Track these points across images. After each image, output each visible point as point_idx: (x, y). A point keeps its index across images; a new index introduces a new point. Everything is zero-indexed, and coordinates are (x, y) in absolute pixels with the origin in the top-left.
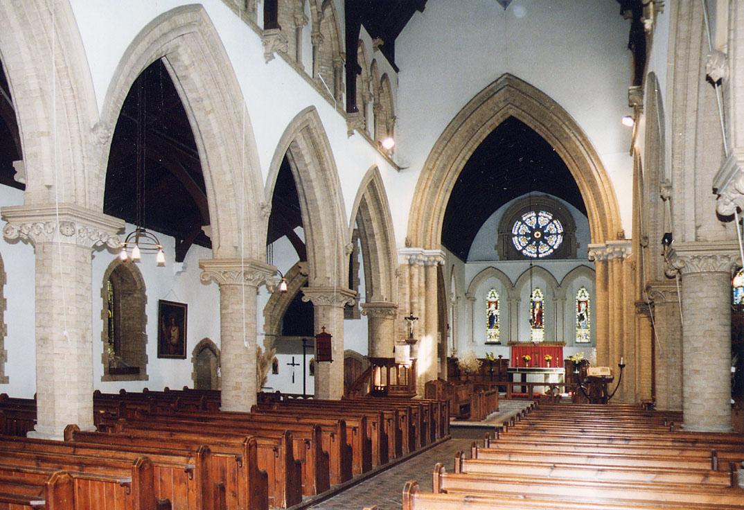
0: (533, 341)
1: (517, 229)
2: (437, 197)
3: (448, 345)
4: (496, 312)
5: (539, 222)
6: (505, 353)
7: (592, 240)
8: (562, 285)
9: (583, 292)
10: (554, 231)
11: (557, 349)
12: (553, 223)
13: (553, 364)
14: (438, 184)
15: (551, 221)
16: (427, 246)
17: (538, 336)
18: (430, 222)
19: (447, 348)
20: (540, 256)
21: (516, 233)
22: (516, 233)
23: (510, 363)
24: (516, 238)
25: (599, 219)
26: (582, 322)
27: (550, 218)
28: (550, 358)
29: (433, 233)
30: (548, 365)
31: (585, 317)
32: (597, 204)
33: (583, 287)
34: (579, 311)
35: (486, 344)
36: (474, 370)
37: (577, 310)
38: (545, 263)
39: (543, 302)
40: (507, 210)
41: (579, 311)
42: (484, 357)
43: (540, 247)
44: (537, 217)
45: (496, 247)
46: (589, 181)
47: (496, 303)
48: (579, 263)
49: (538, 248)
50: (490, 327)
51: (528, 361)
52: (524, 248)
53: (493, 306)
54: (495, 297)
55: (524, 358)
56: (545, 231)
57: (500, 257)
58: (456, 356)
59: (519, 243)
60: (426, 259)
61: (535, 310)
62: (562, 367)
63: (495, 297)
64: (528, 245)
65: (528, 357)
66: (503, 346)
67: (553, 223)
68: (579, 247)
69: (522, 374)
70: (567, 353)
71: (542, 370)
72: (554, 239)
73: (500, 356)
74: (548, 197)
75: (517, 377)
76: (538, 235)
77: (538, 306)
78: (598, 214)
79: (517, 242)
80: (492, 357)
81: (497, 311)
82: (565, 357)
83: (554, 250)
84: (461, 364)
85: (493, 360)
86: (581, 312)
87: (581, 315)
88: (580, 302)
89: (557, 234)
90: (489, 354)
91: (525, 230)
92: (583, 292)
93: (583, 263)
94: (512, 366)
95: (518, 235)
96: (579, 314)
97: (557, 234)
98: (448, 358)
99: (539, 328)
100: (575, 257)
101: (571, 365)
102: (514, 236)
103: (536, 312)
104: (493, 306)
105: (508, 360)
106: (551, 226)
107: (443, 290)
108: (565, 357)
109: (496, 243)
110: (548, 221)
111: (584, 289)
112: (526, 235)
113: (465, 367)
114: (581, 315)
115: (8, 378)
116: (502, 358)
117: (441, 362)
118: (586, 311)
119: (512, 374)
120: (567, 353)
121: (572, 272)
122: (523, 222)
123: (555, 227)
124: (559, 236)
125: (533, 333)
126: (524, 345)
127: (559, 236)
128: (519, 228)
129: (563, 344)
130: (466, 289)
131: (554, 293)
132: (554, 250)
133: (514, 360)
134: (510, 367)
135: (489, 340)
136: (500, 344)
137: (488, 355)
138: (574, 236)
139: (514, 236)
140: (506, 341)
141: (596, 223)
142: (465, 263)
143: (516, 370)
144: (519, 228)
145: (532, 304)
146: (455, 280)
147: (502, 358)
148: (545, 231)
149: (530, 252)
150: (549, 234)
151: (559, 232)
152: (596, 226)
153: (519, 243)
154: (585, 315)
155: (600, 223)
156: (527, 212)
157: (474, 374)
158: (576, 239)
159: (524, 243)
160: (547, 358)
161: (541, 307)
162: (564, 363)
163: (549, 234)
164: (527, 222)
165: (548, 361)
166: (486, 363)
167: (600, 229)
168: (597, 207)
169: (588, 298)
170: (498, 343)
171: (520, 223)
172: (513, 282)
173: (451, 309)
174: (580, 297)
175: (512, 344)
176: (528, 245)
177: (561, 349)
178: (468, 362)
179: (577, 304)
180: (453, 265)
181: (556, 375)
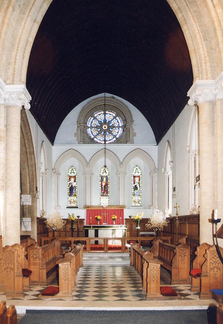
0: (102, 205)
1: (90, 123)
2: (23, 24)
3: (38, 206)
4: (74, 184)
5: (106, 118)
6: (82, 214)
7: (205, 77)
8: (123, 163)
9: (137, 169)
10: (116, 125)
11: (120, 211)
12: (116, 119)
13: (118, 223)
14: (45, 255)
15: (115, 117)
16: (8, 82)
17: (105, 202)
18: (14, 54)
19: (36, 209)
20: (107, 142)
21: (89, 126)
22: (89, 126)
23: (85, 221)
24: (89, 129)
25: (206, 54)
26: (136, 191)
27: (114, 115)
28: (116, 217)
29: (16, 67)
30: (99, 223)
31: (138, 187)
32: (204, 37)
33: (137, 166)
34: (134, 183)
35: (67, 208)
36: (59, 228)
37: (133, 182)
38: (111, 146)
39: (109, 176)
40: (84, 107)
41: (134, 183)
42: (66, 217)
43: (106, 136)
44: (105, 114)
45: (76, 135)
46: (195, 12)
47: (75, 177)
48: (136, 147)
49: (105, 137)
50: (70, 195)
51: (99, 220)
52: (95, 137)
53: (72, 179)
54: (74, 173)
55: (97, 218)
56: (110, 125)
57: (78, 142)
58: (44, 217)
59: (92, 133)
60: (7, 96)
61: (103, 182)
62: (123, 224)
63: (74, 173)
64: (98, 134)
65: (99, 217)
66: (80, 209)
67: (116, 119)
68: (135, 136)
69: (95, 230)
70: (127, 214)
71: (110, 227)
72: (117, 130)
73: (78, 217)
74: (114, 98)
75: (91, 233)
76: (105, 127)
77: (105, 179)
78: (205, 48)
79: (90, 132)
80: (73, 217)
81: (75, 183)
82: (126, 216)
83: (117, 139)
84: (48, 223)
85: (74, 219)
86: (136, 184)
87: (136, 186)
88: (134, 177)
89: (119, 127)
90: (71, 215)
91: (95, 123)
92: (137, 169)
93: (139, 147)
94: (87, 224)
95: (91, 127)
96: (134, 185)
97: (119, 127)
98: (38, 218)
99: (106, 196)
100: (133, 143)
101: (131, 222)
102: (89, 127)
103: (104, 184)
104: (72, 179)
105: (84, 220)
106: (115, 121)
107: (33, 157)
108: (126, 216)
109: (76, 132)
110: (113, 117)
111: (138, 167)
112: (97, 127)
113: (52, 225)
114: (136, 186)
115: (210, 222)
116: (80, 218)
117: (32, 221)
118: (139, 183)
119: (88, 230)
120: (127, 214)
121: (126, 158)
122: (95, 118)
123: (118, 122)
124: (120, 129)
125: (101, 199)
126: (97, 208)
127: (120, 129)
128: (92, 122)
129: (124, 207)
130: (53, 165)
131: (117, 169)
132: (117, 139)
133: (88, 220)
134: (85, 224)
135: (69, 205)
136: (78, 208)
137: (70, 216)
138: (132, 126)
139: (89, 127)
140: (82, 206)
141: (203, 58)
142: (53, 145)
143: (90, 227)
144: (92, 122)
145: (100, 178)
146: (44, 152)
147: (80, 218)
148: (110, 125)
149: (100, 140)
150: (113, 127)
151: (120, 125)
152: (203, 62)
153: (92, 133)
154: (138, 186)
155: (207, 58)
156: (97, 110)
157: (59, 231)
158: (133, 130)
159: (95, 133)
160: (113, 218)
161: (107, 180)
162: (125, 221)
163: (113, 127)
164: (97, 118)
165: (114, 219)
166: (69, 222)
167: (208, 64)
168: (204, 40)
169: (140, 174)
170: (76, 207)
171: (92, 118)
172: (88, 161)
173: (41, 178)
174: (135, 173)
175: (86, 207)
176: (98, 134)
177: (123, 210)
178: (54, 221)
179: (133, 178)
180: (43, 141)
181: (120, 231)
